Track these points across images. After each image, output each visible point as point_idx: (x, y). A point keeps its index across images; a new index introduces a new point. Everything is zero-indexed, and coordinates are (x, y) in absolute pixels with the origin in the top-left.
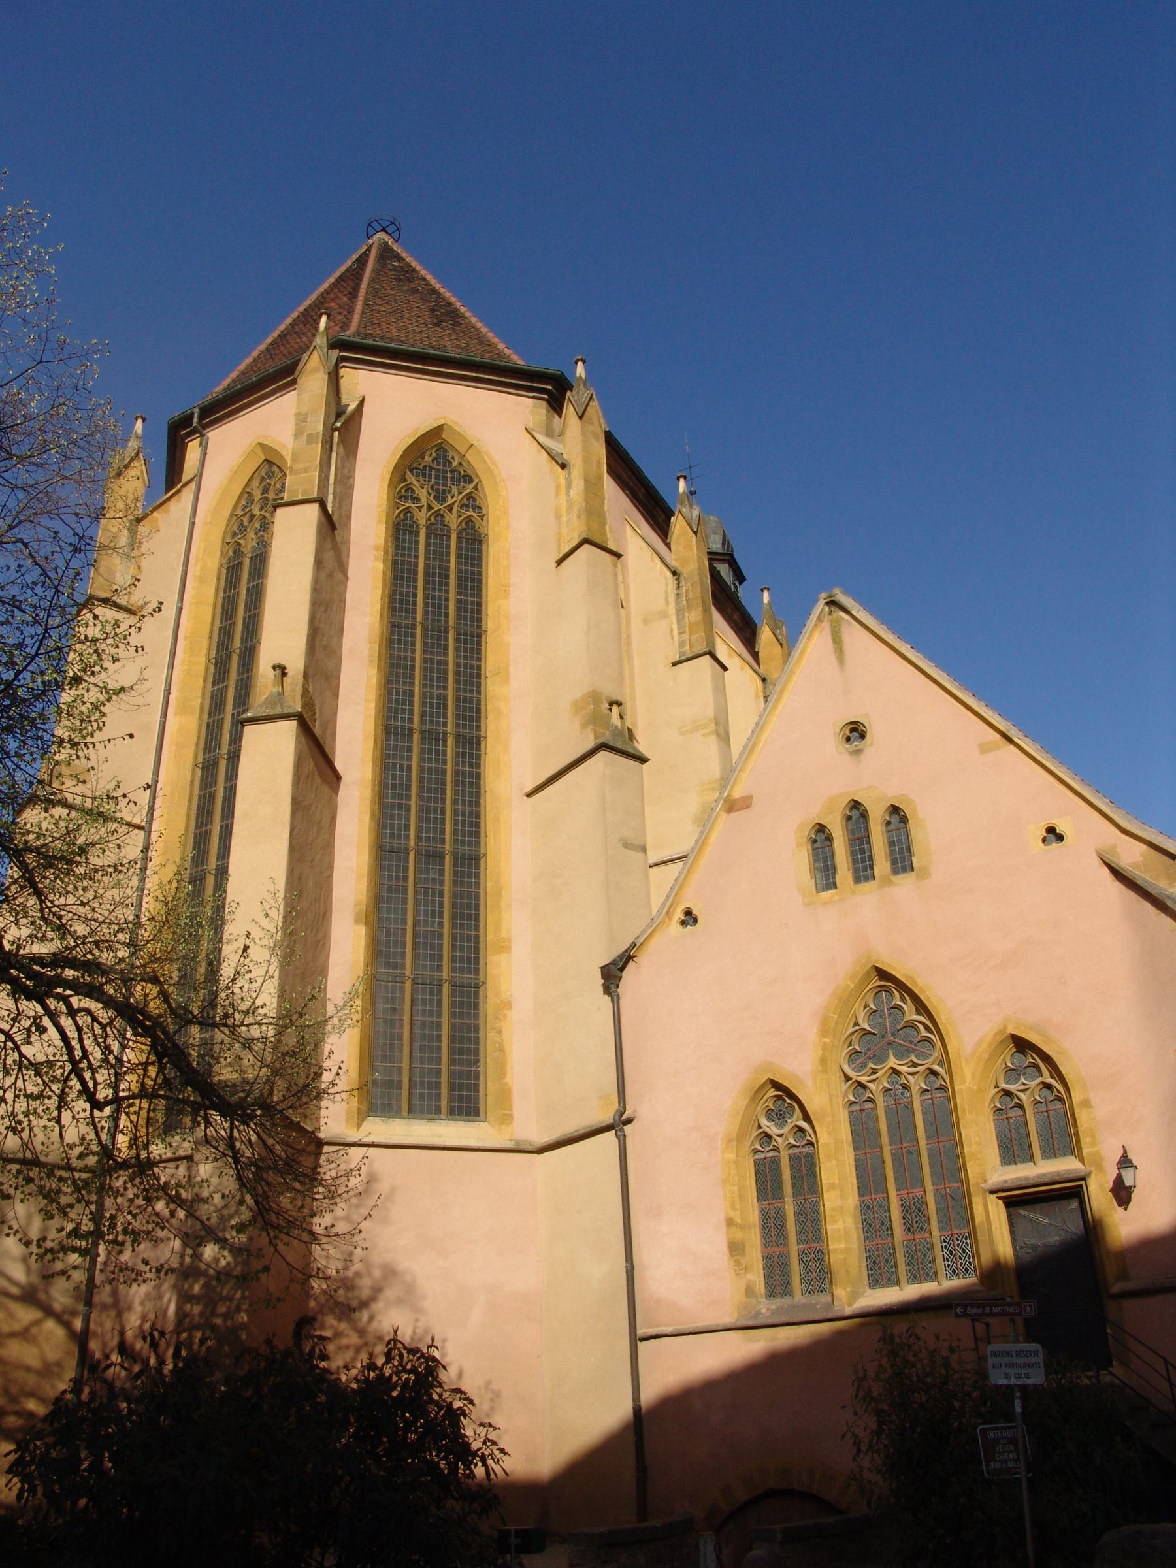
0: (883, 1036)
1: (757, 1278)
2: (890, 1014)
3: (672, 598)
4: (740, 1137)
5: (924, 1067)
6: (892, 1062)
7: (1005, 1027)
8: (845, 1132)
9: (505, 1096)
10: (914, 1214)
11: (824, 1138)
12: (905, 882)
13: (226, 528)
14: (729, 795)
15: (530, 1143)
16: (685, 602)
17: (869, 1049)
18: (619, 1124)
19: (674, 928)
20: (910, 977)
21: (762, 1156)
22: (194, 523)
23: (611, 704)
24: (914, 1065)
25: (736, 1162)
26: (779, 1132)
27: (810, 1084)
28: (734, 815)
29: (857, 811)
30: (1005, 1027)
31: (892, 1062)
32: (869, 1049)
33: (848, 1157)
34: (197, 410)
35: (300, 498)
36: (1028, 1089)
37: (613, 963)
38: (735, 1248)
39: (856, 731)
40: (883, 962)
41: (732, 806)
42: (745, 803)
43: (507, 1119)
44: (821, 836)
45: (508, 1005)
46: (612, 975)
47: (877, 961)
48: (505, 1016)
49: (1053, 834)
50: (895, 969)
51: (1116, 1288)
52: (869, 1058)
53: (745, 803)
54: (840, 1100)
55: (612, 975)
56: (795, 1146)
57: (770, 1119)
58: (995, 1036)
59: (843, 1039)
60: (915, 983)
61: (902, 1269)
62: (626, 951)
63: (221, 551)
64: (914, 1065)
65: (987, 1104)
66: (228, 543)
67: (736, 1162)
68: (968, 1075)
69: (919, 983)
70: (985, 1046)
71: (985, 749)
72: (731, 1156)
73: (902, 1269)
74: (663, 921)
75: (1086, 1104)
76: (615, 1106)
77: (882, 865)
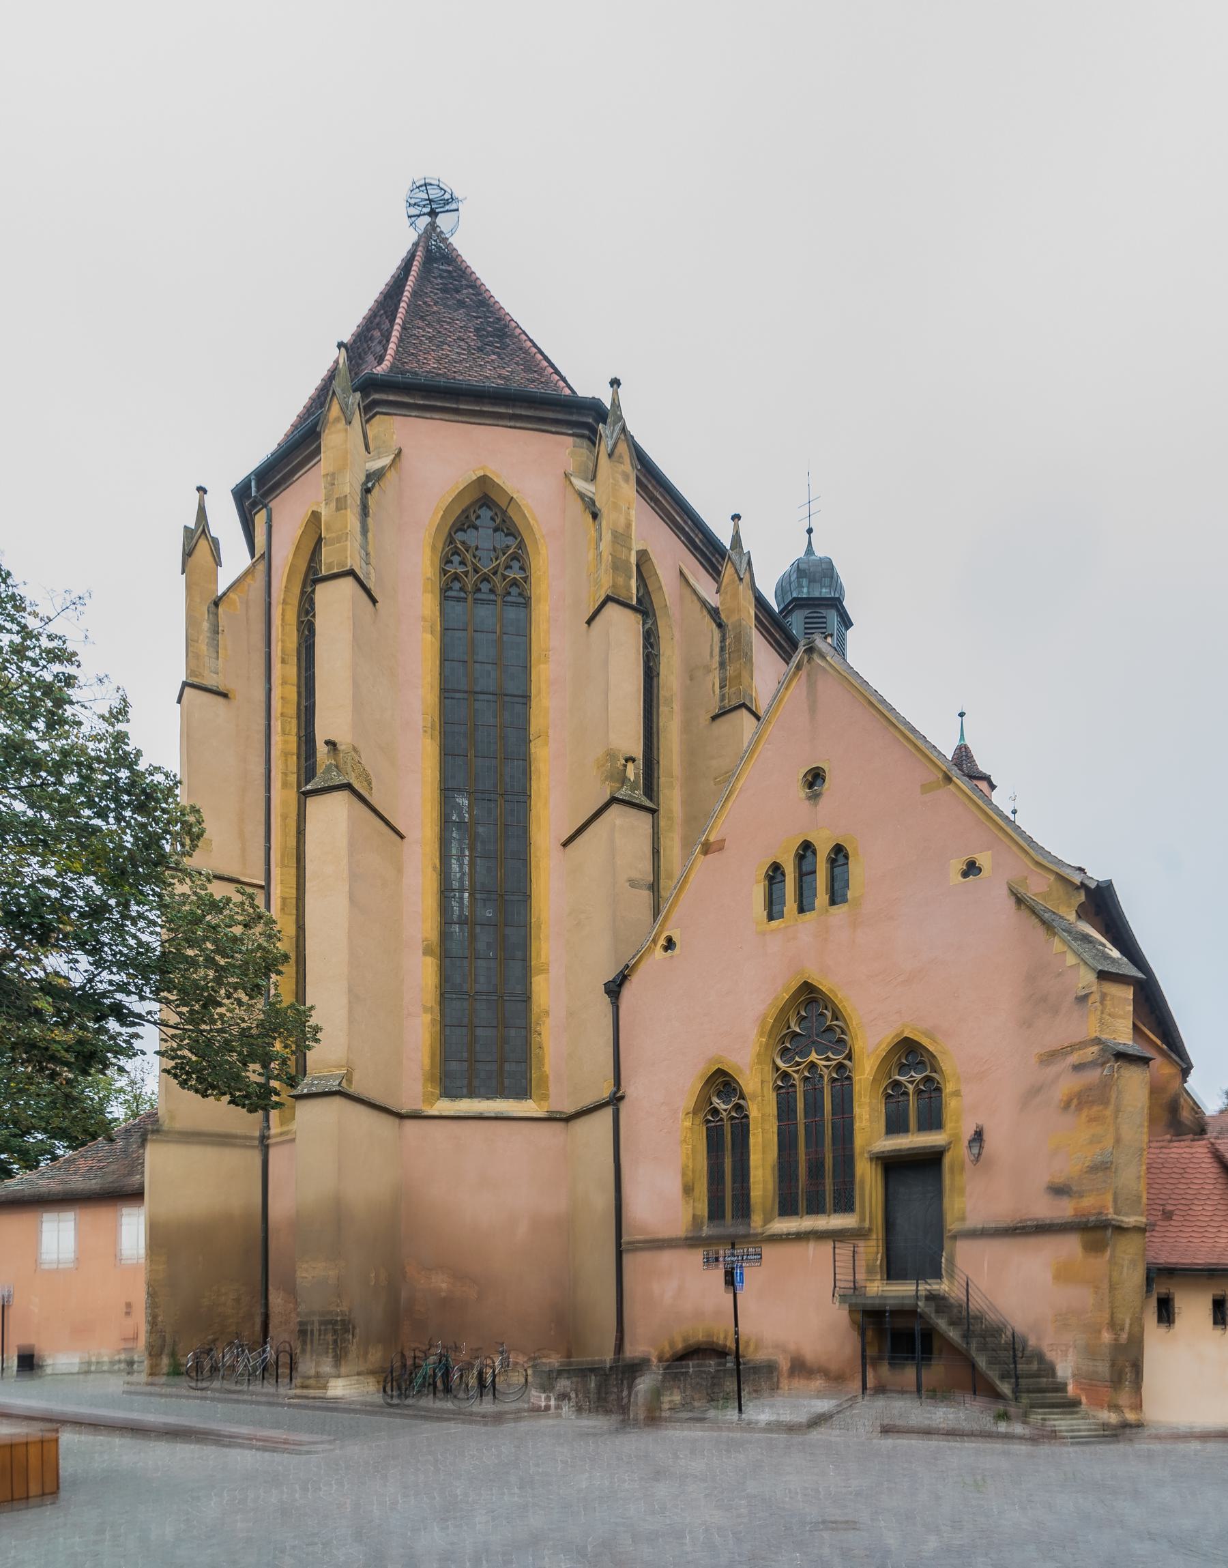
0: (810, 1037)
1: (703, 1208)
2: (817, 1020)
3: (717, 650)
4: (695, 1112)
5: (834, 1063)
6: (814, 1057)
7: (902, 1032)
8: (772, 1109)
9: (544, 1080)
10: (816, 1169)
11: (754, 1112)
12: (840, 910)
13: (299, 606)
14: (707, 840)
15: (561, 1112)
16: (727, 655)
17: (797, 1047)
18: (616, 1100)
19: (659, 952)
20: (833, 991)
21: (713, 1124)
22: (270, 603)
23: (627, 760)
24: (828, 1059)
25: (691, 1129)
26: (725, 1107)
27: (748, 1072)
28: (709, 856)
29: (806, 849)
30: (902, 1032)
31: (814, 1057)
32: (797, 1047)
33: (772, 1127)
34: (253, 477)
35: (336, 571)
36: (910, 1080)
37: (613, 981)
38: (688, 1190)
39: (815, 778)
40: (813, 979)
41: (707, 849)
42: (720, 846)
43: (545, 1097)
44: (775, 873)
45: (547, 1013)
46: (614, 989)
47: (808, 978)
48: (544, 1023)
49: (972, 869)
50: (822, 984)
52: (797, 1053)
53: (720, 846)
54: (771, 1084)
55: (614, 989)
56: (736, 1118)
57: (719, 1096)
58: (893, 1038)
59: (778, 1039)
60: (836, 995)
61: (829, 1201)
62: (621, 971)
63: (298, 630)
64: (798, 1064)
65: (881, 1090)
66: (303, 622)
67: (691, 1129)
68: (868, 1069)
69: (839, 996)
70: (884, 1046)
71: (926, 788)
72: (688, 1124)
73: (829, 1201)
74: (649, 948)
75: (957, 1093)
76: (612, 1089)
77: (822, 897)
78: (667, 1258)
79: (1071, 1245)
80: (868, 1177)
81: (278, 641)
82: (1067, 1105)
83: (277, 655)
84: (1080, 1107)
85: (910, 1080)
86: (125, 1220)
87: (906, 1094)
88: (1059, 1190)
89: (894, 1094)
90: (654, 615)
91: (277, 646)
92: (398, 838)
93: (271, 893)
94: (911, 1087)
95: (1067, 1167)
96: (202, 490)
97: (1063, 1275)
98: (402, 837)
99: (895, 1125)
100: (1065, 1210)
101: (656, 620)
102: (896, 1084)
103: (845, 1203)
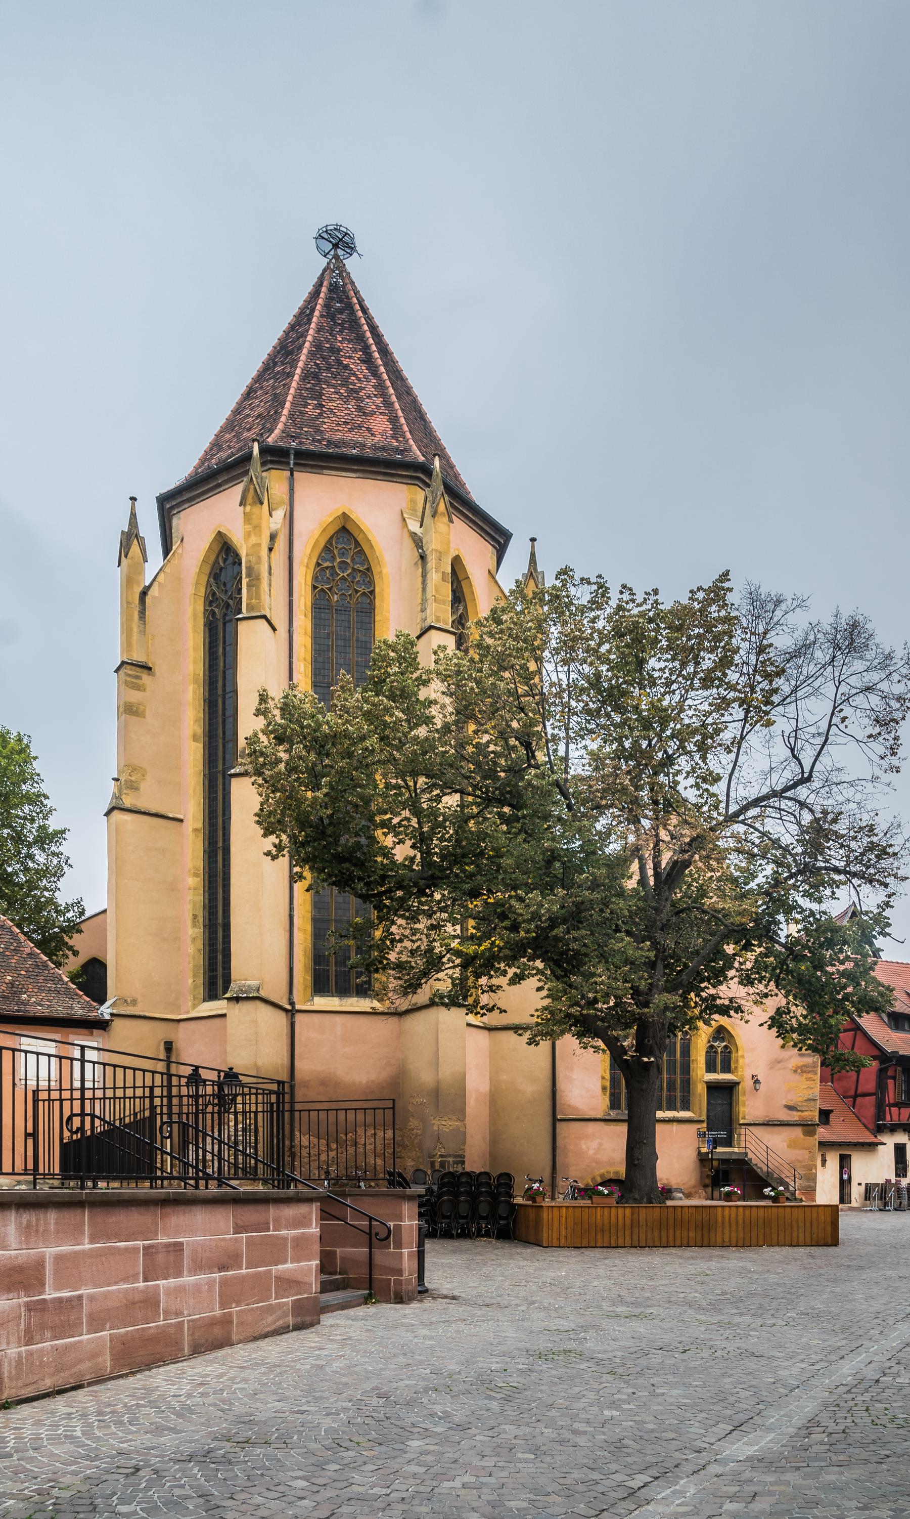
36: (719, 1045)
51: (742, 1122)
75: (743, 1057)
78: (591, 1127)
79: (798, 1132)
80: (700, 1091)
81: (301, 596)
82: (795, 1071)
83: (299, 607)
84: (802, 1072)
85: (719, 1045)
86: (440, 1015)
87: (716, 1052)
88: (790, 1108)
89: (711, 1050)
90: (465, 601)
91: (300, 600)
92: (178, 824)
93: (233, 849)
94: (719, 1050)
95: (794, 1098)
96: (533, 540)
97: (792, 1145)
98: (181, 821)
99: (711, 1068)
100: (795, 1116)
101: (466, 607)
102: (712, 1047)
103: (686, 1107)
